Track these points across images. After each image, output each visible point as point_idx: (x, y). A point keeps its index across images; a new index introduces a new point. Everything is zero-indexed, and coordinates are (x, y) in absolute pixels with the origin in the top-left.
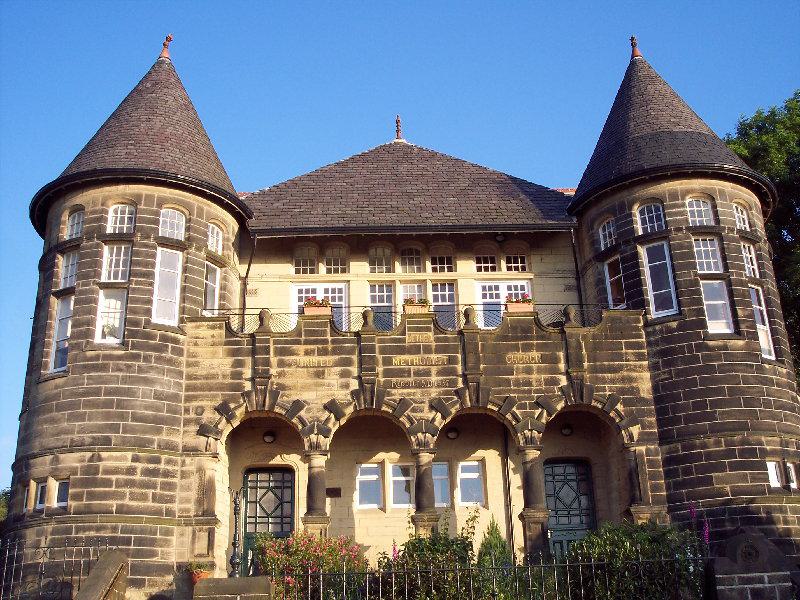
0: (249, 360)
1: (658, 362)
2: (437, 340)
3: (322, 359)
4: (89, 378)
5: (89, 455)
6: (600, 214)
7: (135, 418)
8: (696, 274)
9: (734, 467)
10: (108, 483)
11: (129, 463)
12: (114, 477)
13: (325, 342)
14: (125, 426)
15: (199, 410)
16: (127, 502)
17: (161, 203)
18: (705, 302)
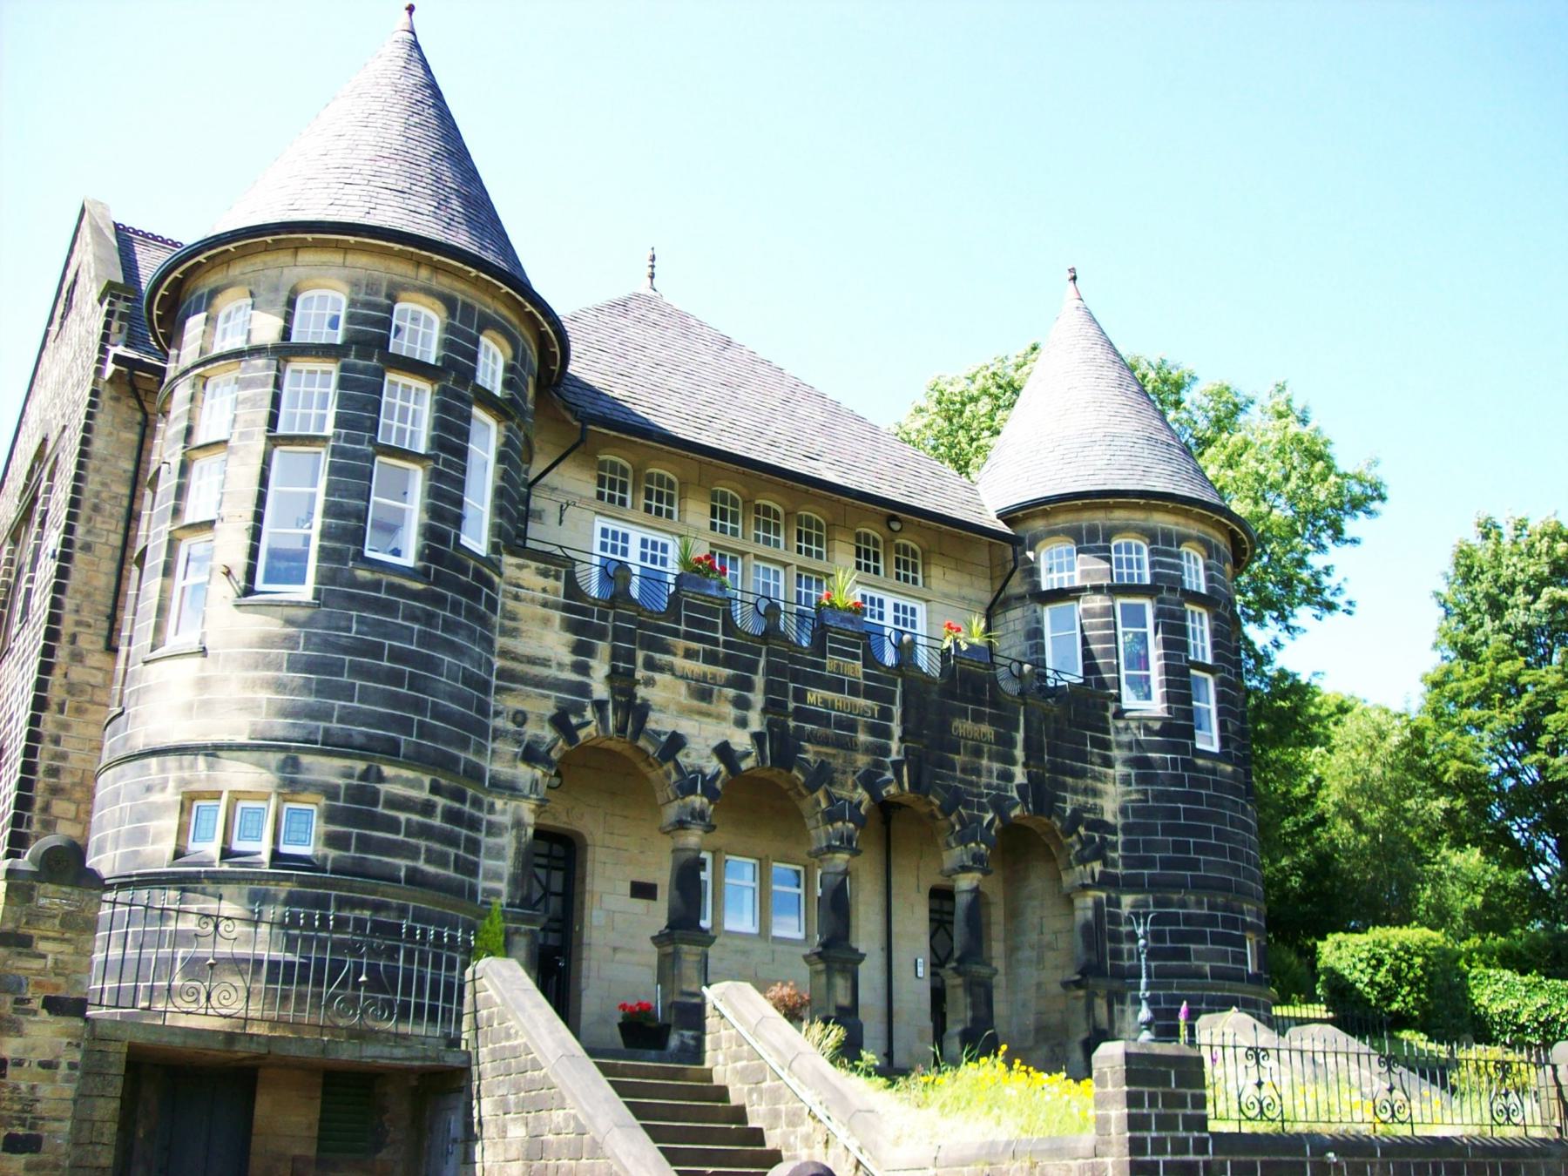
0: (603, 648)
1: (1129, 775)
2: (867, 676)
3: (710, 669)
4: (361, 621)
5: (360, 766)
6: (1053, 533)
7: (438, 713)
8: (1187, 660)
9: (1217, 939)
10: (393, 825)
11: (424, 795)
12: (403, 816)
13: (715, 642)
14: (421, 724)
15: (519, 718)
16: (421, 864)
17: (1183, 539)
18: (373, 498)
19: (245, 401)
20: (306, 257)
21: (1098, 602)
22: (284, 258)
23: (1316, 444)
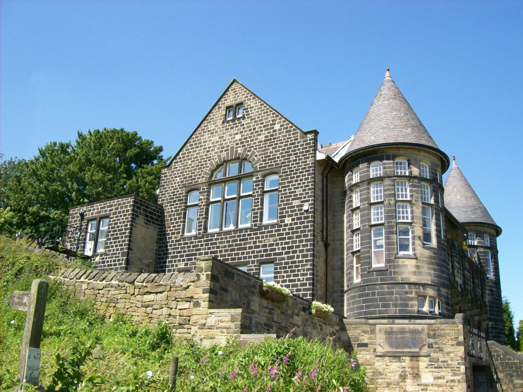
14: (153, 220)
19: (415, 191)
20: (422, 153)
21: (482, 250)
22: (416, 152)
23: (207, 123)
